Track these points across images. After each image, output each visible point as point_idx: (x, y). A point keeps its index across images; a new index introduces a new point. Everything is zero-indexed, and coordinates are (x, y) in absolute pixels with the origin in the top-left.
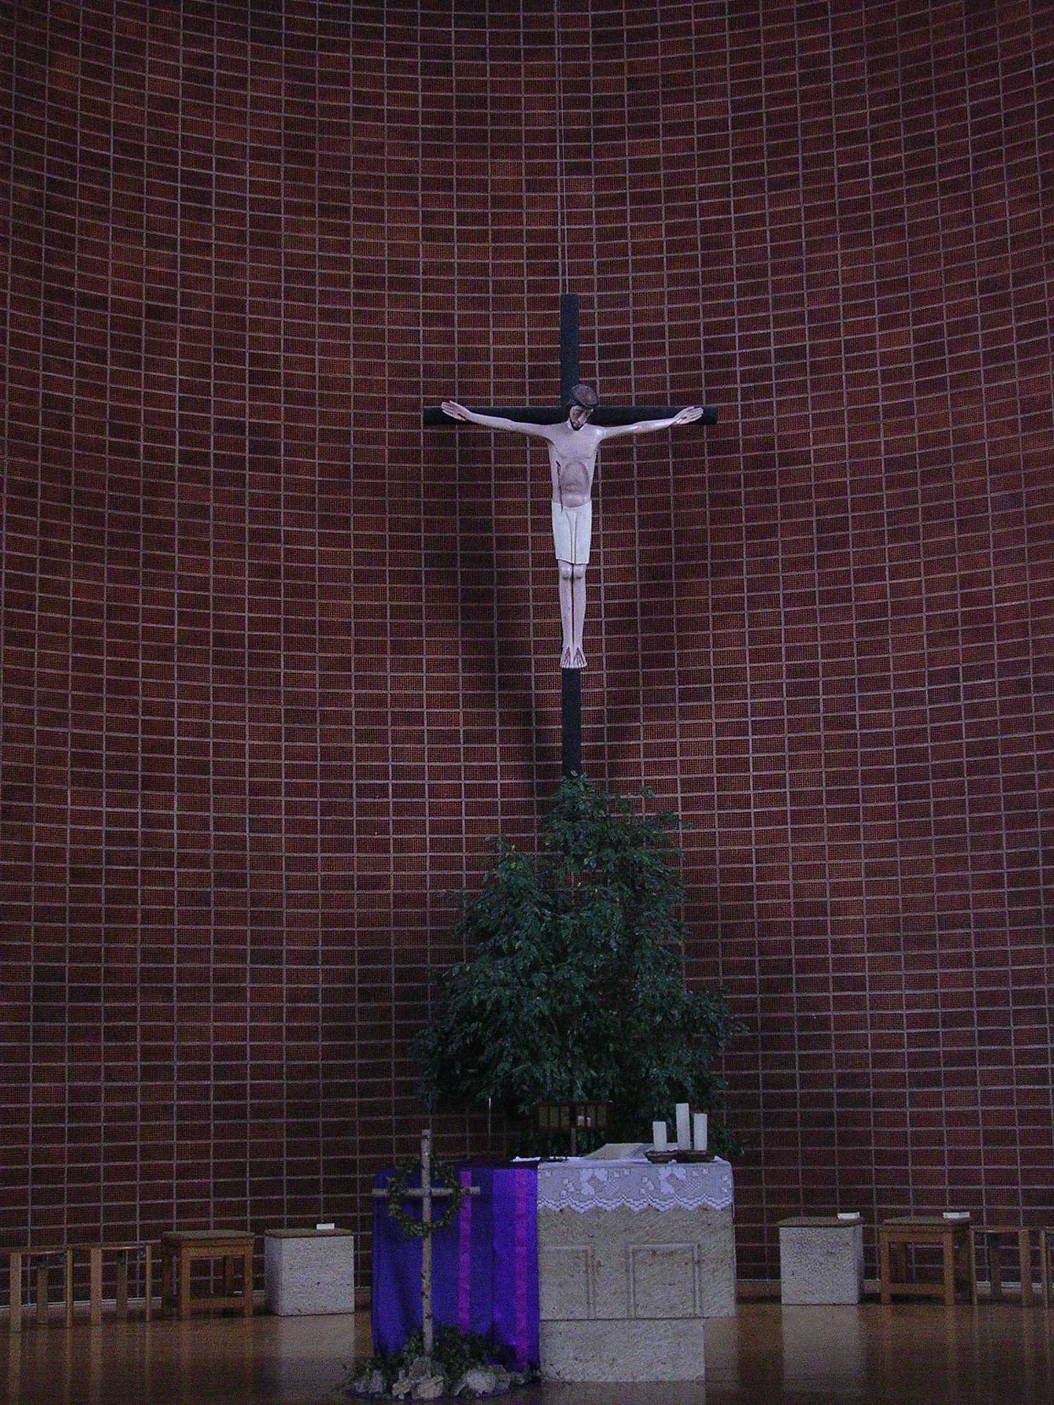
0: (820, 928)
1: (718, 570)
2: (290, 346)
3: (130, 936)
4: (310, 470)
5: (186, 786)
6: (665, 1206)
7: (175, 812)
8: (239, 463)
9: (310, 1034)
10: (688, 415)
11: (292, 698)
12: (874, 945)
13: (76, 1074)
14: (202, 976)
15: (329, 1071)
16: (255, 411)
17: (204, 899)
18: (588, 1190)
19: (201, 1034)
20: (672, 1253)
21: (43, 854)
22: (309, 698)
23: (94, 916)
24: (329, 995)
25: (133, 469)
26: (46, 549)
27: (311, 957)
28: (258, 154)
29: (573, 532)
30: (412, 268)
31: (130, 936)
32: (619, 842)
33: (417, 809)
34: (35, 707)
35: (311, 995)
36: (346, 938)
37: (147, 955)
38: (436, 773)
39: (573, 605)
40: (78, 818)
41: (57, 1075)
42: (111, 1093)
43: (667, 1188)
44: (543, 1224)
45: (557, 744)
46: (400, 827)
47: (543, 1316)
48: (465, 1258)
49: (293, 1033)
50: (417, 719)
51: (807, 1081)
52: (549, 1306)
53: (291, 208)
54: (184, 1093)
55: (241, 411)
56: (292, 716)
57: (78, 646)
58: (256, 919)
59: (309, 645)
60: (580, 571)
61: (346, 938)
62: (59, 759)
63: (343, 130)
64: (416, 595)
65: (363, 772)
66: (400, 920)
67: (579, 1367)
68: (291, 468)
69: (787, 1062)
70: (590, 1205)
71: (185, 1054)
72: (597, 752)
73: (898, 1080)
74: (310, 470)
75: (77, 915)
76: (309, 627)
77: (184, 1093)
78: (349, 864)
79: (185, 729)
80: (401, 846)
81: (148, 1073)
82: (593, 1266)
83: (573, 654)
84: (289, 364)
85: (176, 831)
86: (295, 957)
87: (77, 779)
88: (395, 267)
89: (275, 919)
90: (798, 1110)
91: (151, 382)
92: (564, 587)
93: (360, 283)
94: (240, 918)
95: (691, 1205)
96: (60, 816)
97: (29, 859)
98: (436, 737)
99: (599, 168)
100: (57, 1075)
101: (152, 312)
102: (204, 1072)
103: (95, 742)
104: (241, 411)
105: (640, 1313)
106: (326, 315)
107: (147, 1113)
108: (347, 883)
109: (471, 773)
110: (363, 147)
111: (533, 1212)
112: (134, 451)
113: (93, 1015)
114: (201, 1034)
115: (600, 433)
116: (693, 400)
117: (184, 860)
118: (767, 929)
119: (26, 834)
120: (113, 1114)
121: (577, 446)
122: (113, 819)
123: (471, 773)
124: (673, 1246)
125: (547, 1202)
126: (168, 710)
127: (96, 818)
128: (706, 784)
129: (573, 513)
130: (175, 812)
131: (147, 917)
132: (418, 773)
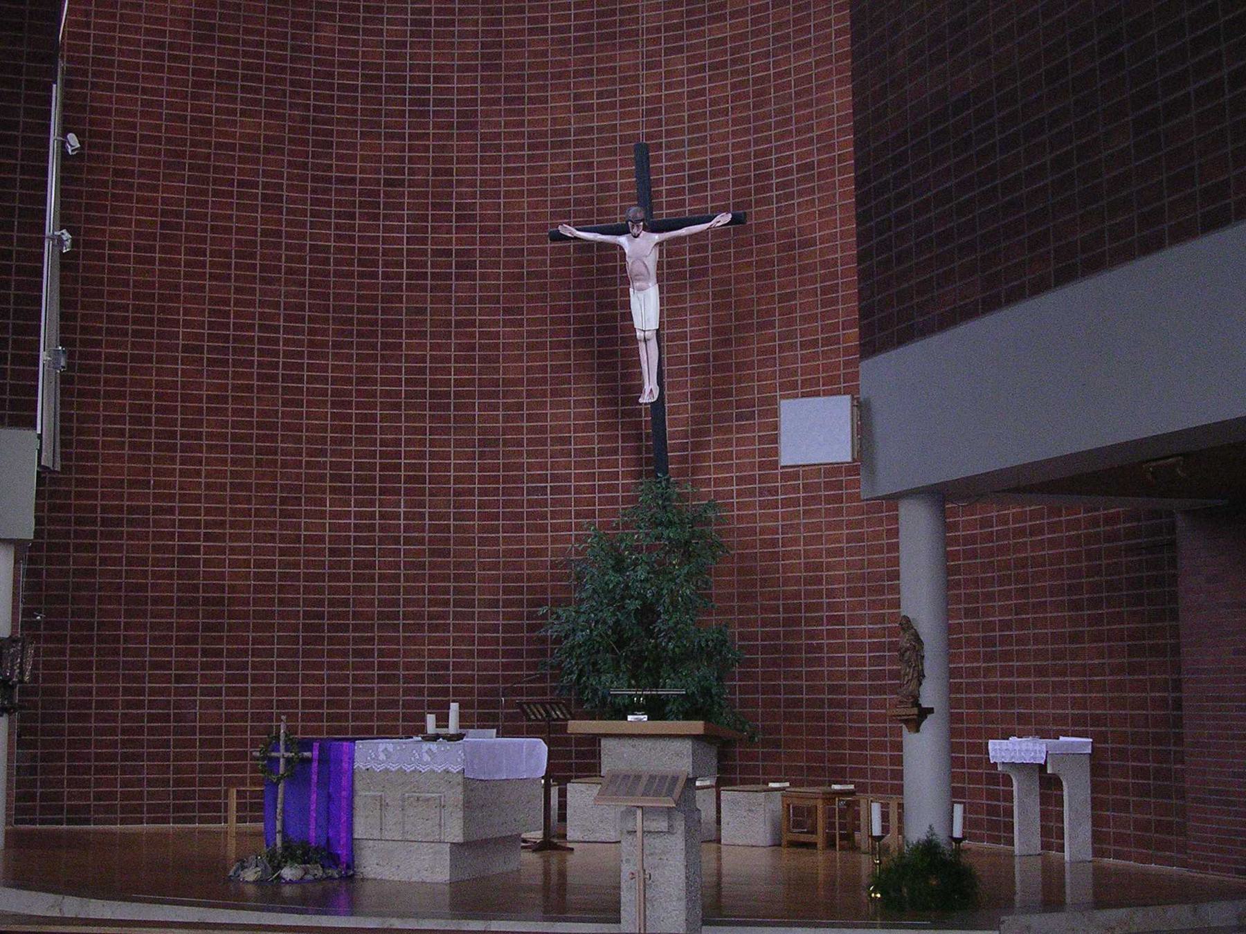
0: (819, 581)
1: (761, 326)
2: (484, 195)
3: (371, 590)
4: (497, 277)
5: (408, 492)
6: (425, 769)
7: (402, 510)
8: (448, 277)
9: (494, 654)
10: (723, 219)
11: (483, 431)
12: (852, 592)
13: (331, 679)
14: (420, 616)
15: (506, 679)
16: (460, 241)
17: (421, 566)
18: (382, 757)
19: (419, 654)
20: (428, 800)
21: (309, 539)
22: (494, 431)
23: (346, 578)
24: (507, 629)
25: (374, 287)
26: (312, 344)
27: (495, 603)
28: (463, 69)
29: (646, 307)
30: (566, 132)
31: (371, 590)
32: (670, 521)
33: (566, 503)
34: (304, 446)
35: (495, 628)
36: (519, 591)
37: (383, 603)
38: (579, 477)
39: (649, 357)
40: (335, 515)
41: (319, 679)
42: (356, 691)
43: (426, 758)
44: (357, 778)
45: (647, 440)
46: (554, 515)
47: (356, 836)
48: (314, 797)
49: (483, 654)
50: (567, 441)
51: (811, 689)
52: (359, 832)
53: (485, 102)
54: (407, 692)
55: (449, 242)
56: (483, 443)
57: (334, 405)
58: (457, 578)
59: (496, 395)
60: (651, 335)
61: (519, 591)
62: (322, 478)
63: (521, 44)
64: (567, 356)
65: (531, 479)
66: (554, 578)
67: (379, 870)
68: (484, 277)
69: (798, 677)
70: (382, 767)
71: (407, 666)
72: (684, 459)
73: (862, 690)
74: (497, 277)
75: (333, 577)
76: (496, 383)
77: (407, 692)
78: (521, 541)
79: (409, 455)
80: (555, 528)
81: (382, 679)
82: (383, 806)
83: (650, 391)
84: (482, 206)
85: (402, 522)
86: (483, 603)
87: (334, 490)
88: (555, 133)
89: (470, 578)
90: (803, 710)
91: (387, 229)
92: (642, 346)
93: (531, 147)
94: (446, 578)
95: (439, 769)
96: (322, 515)
97: (299, 542)
98: (579, 452)
99: (690, 47)
100: (319, 679)
101: (388, 183)
102: (421, 679)
103: (347, 466)
104: (449, 242)
105: (409, 837)
106: (508, 171)
107: (381, 705)
108: (519, 553)
109: (603, 476)
110: (535, 54)
111: (352, 772)
112: (374, 275)
113: (344, 641)
114: (419, 654)
115: (657, 237)
116: (725, 209)
117: (408, 541)
118: (787, 582)
119: (297, 526)
120: (357, 705)
121: (641, 249)
122: (359, 515)
123: (603, 476)
124: (429, 795)
125: (359, 764)
126: (397, 443)
127: (347, 515)
128: (752, 480)
129: (641, 295)
130: (402, 510)
131: (382, 578)
132: (567, 478)
